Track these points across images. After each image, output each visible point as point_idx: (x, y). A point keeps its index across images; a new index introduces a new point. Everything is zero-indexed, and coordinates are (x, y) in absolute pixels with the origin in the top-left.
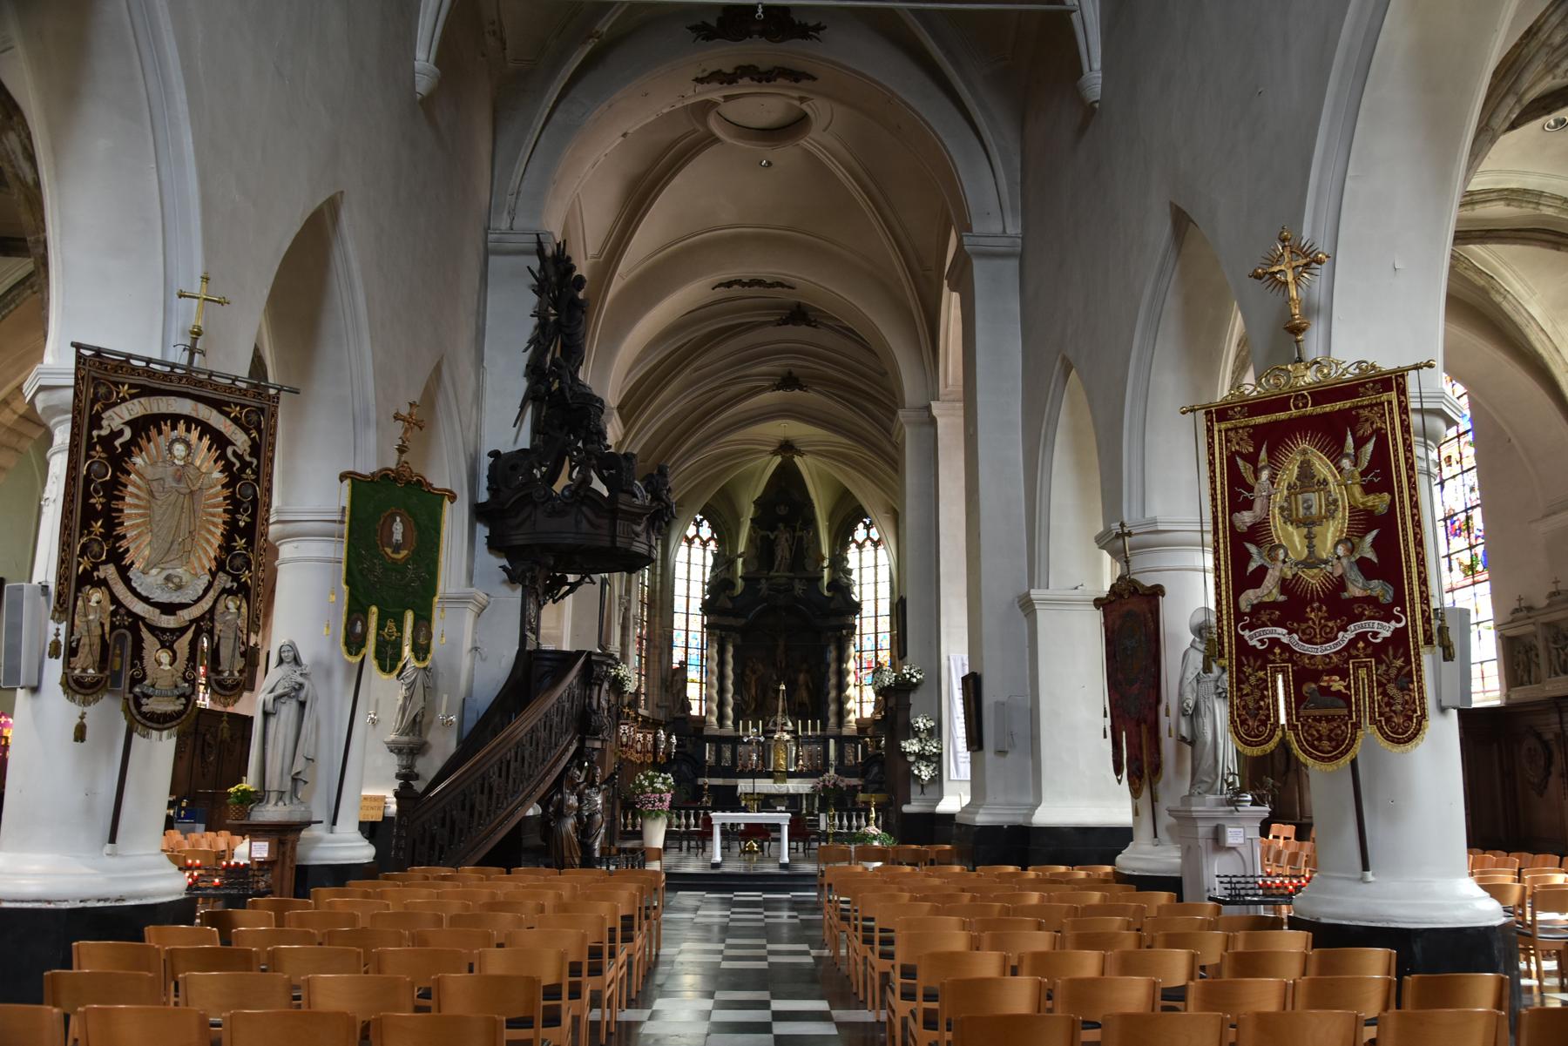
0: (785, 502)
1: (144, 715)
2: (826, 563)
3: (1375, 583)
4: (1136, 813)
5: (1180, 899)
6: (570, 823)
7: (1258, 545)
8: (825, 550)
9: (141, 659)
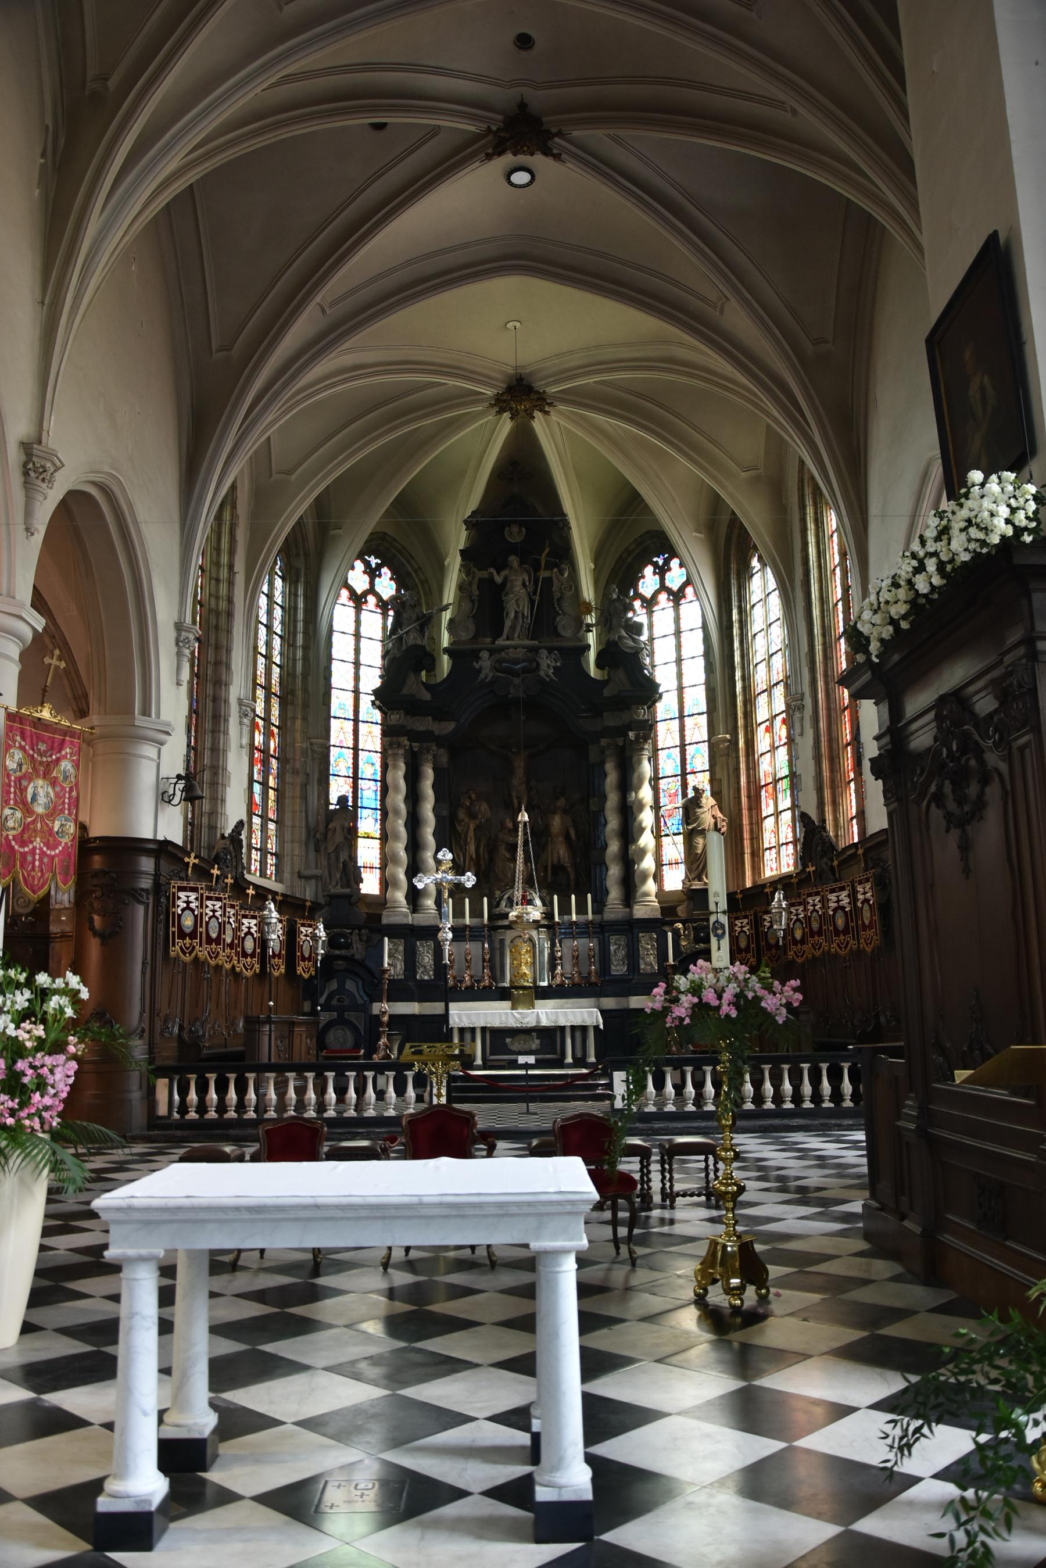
0: (520, 515)
8: (588, 592)
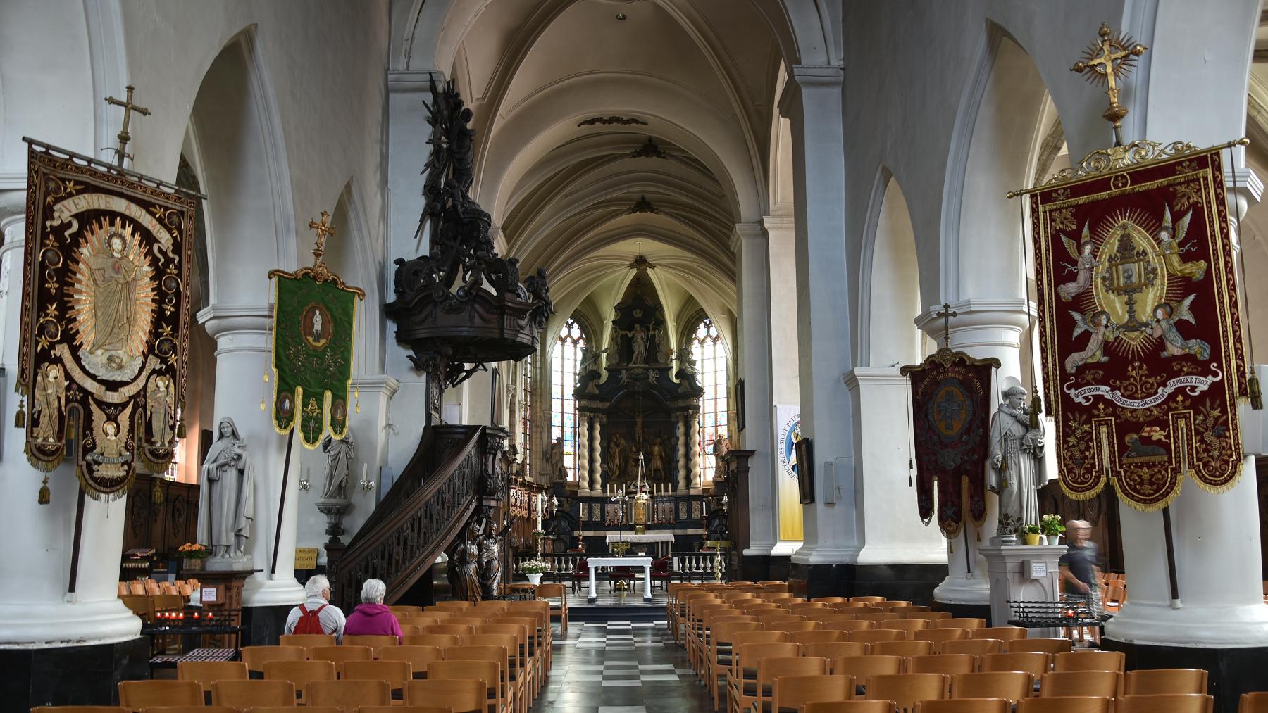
0: (640, 308)
1: (95, 479)
2: (674, 356)
3: (1193, 342)
4: (951, 551)
5: (989, 624)
6: (472, 568)
7: (1082, 312)
8: (673, 345)
9: (91, 430)
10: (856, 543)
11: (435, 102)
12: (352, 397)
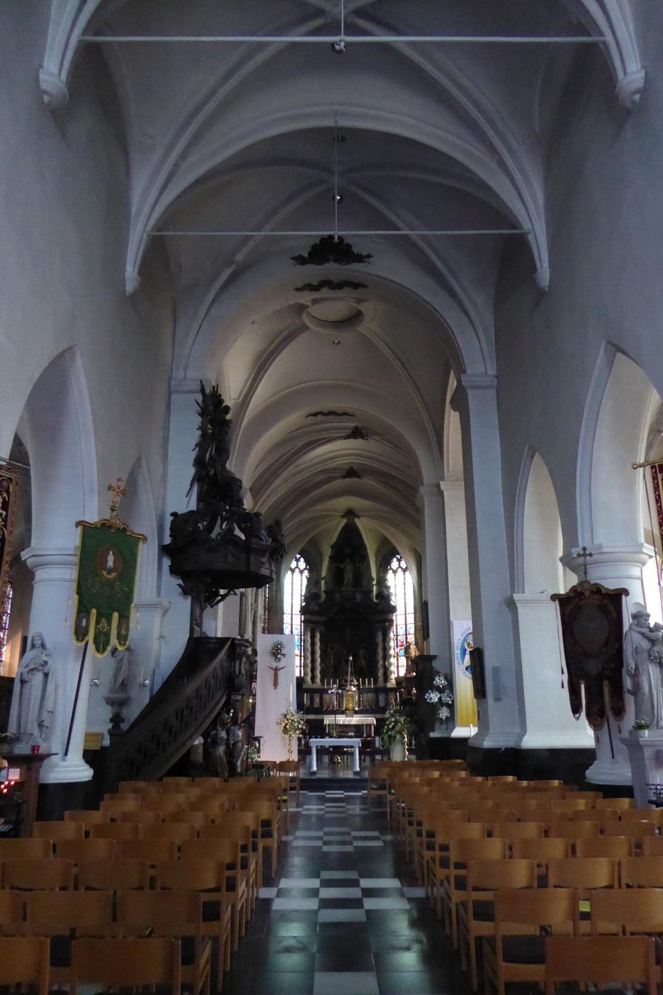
4: (597, 740)
6: (221, 750)
8: (374, 575)
10: (518, 730)
11: (204, 400)
12: (135, 616)
